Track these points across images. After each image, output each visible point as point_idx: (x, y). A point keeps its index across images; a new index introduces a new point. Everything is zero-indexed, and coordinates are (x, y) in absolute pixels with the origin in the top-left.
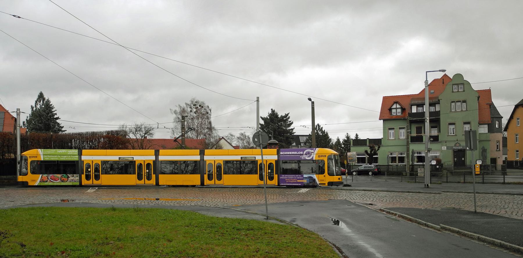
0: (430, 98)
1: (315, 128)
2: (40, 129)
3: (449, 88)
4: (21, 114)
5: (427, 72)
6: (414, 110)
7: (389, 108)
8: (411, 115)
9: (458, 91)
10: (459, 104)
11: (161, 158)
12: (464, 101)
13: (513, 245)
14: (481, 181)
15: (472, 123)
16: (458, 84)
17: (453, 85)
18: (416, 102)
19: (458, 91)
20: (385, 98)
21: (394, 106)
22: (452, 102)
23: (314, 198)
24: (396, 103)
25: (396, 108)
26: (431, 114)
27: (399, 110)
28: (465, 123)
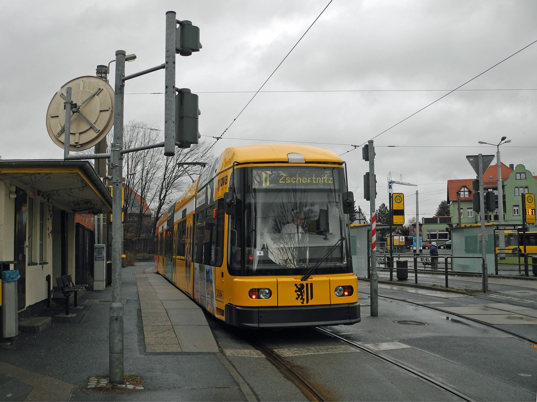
2: (190, 279)
3: (512, 175)
4: (41, 266)
5: (390, 183)
7: (457, 190)
12: (526, 187)
16: (520, 173)
17: (516, 173)
18: (491, 186)
20: (450, 183)
21: (463, 190)
23: (118, 371)
24: (464, 187)
25: (464, 191)
27: (467, 193)
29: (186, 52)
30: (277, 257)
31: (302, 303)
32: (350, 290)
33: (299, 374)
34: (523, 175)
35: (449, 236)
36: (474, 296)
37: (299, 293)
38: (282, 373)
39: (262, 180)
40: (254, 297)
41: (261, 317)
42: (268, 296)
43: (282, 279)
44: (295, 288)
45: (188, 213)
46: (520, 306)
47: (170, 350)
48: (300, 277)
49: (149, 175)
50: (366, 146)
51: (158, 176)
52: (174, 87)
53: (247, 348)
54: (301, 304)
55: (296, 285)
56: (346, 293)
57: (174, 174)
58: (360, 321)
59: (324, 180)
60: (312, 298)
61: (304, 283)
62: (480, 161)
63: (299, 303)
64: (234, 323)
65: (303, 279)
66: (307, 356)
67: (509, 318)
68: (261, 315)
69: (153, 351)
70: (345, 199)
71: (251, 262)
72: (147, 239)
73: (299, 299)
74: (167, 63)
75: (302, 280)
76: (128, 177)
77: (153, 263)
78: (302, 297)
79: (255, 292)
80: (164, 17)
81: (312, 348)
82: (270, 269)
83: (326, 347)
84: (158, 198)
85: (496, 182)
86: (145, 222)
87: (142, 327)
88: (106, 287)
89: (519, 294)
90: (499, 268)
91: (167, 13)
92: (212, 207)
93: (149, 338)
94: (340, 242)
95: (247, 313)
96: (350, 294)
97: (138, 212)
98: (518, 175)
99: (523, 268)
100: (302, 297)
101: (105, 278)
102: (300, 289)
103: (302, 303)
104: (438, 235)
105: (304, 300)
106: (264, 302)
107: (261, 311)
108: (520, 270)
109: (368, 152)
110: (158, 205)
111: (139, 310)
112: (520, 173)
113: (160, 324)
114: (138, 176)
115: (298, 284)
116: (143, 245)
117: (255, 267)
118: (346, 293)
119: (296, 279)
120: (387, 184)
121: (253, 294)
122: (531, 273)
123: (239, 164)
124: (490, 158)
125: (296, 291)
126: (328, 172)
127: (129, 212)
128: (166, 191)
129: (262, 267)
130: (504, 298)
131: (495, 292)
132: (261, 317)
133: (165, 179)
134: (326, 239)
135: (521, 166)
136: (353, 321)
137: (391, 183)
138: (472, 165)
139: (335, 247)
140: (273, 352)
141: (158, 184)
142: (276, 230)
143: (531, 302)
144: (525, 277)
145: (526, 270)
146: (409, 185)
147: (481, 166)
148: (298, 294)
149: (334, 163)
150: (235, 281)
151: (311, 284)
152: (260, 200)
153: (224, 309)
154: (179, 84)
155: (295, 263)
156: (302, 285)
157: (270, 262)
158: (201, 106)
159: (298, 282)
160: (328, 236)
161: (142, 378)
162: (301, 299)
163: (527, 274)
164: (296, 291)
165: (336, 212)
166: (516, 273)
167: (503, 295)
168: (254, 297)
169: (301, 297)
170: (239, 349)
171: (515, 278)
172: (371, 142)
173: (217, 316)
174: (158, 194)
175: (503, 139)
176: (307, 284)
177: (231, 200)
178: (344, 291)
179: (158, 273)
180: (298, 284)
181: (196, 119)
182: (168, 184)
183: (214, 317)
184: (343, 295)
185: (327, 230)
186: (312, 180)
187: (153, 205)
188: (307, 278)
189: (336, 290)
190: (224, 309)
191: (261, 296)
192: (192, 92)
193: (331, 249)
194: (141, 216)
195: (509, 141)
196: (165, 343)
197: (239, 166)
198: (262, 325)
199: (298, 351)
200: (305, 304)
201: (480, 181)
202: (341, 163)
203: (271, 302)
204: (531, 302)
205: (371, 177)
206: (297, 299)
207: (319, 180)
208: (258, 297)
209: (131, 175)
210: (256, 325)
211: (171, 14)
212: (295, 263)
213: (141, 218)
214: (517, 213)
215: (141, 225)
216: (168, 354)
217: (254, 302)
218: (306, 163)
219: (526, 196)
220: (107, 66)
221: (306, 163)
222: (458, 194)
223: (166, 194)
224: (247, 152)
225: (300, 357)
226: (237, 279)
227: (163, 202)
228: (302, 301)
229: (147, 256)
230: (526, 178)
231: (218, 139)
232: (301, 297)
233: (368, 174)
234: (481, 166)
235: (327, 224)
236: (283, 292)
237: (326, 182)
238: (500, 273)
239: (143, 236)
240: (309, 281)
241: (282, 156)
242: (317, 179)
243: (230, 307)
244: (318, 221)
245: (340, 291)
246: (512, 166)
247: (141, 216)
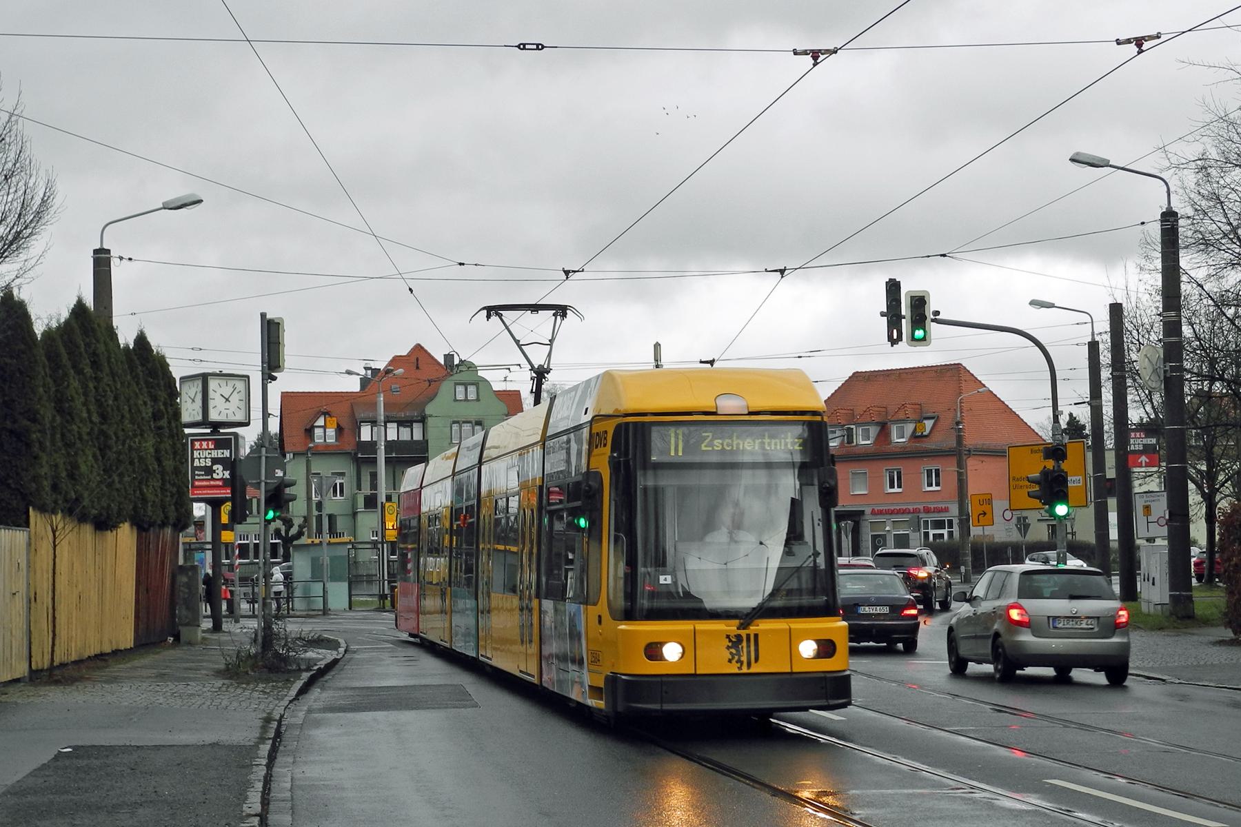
3: (446, 387)
9: (466, 400)
12: (479, 423)
19: (466, 400)
21: (321, 422)
22: (454, 422)
27: (331, 432)
35: (281, 551)
48: (737, 622)
54: (737, 671)
55: (728, 637)
59: (786, 444)
60: (757, 660)
65: (743, 626)
98: (460, 389)
103: (740, 668)
104: (252, 546)
105: (742, 663)
112: (466, 385)
119: (731, 627)
125: (728, 648)
151: (756, 636)
153: (602, 685)
156: (739, 637)
164: (728, 648)
176: (748, 636)
180: (732, 634)
190: (602, 685)
198: (667, 707)
200: (745, 670)
206: (730, 661)
210: (656, 707)
218: (750, 413)
221: (750, 413)
222: (309, 432)
226: (623, 627)
230: (478, 400)
240: (753, 629)
243: (613, 680)
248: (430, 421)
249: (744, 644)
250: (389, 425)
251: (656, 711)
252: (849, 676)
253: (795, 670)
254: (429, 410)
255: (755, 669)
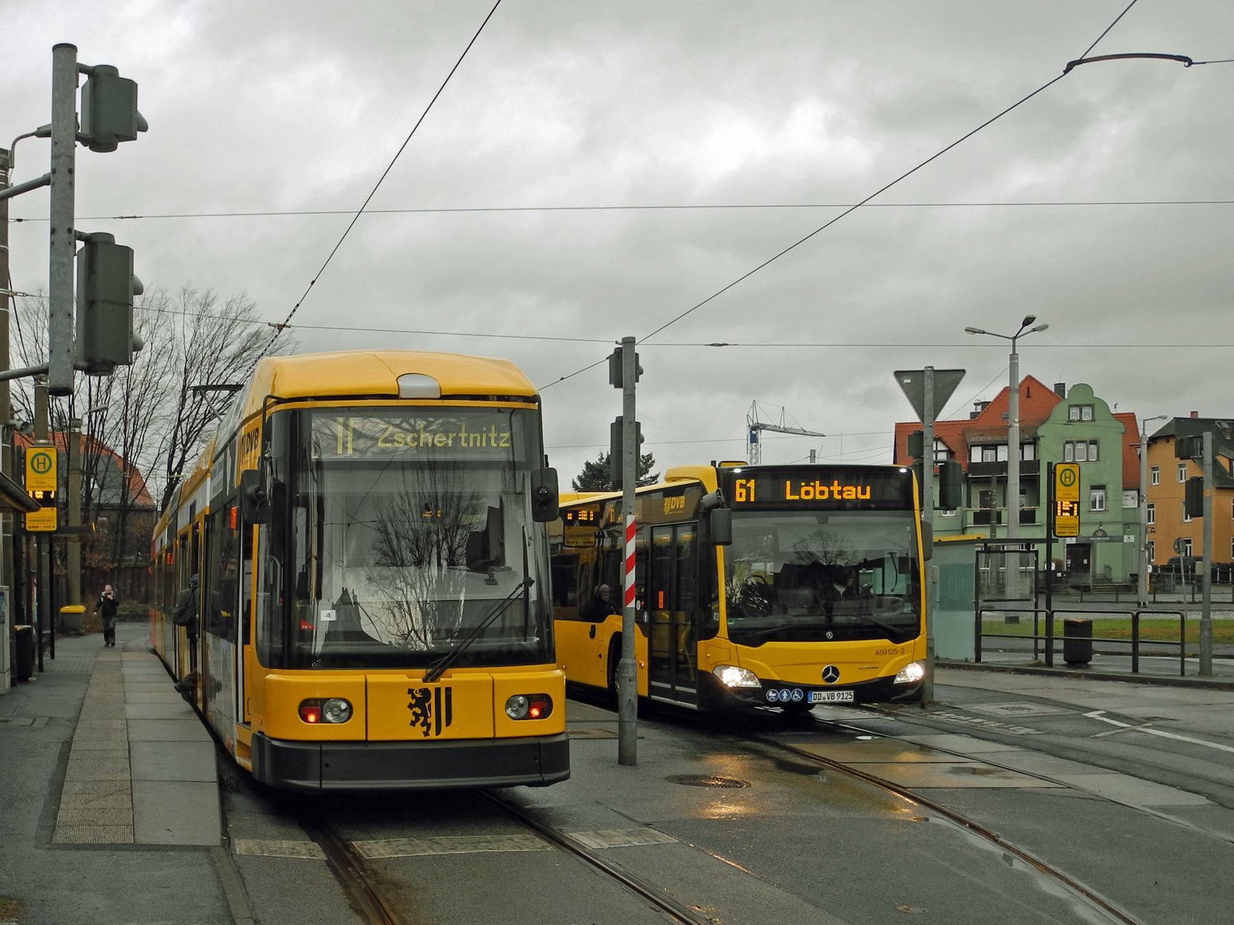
0: (1022, 430)
1: (761, 681)
3: (1059, 412)
6: (977, 456)
8: (974, 467)
9: (1080, 420)
10: (1080, 446)
11: (100, 659)
12: (1094, 442)
13: (679, 703)
14: (1127, 670)
15: (1110, 487)
16: (1080, 407)
17: (1070, 406)
19: (1080, 420)
22: (1068, 442)
26: (1024, 465)
28: (1094, 488)
29: (102, 142)
30: (382, 624)
31: (426, 734)
32: (543, 703)
33: (387, 900)
34: (1086, 410)
36: (896, 715)
37: (418, 711)
38: (349, 895)
39: (336, 439)
40: (312, 718)
41: (327, 765)
42: (344, 715)
43: (377, 677)
44: (409, 699)
45: (198, 510)
46: (995, 741)
47: (108, 840)
48: (422, 672)
49: (143, 412)
50: (618, 352)
51: (164, 413)
52: (70, 231)
53: (285, 837)
54: (422, 737)
55: (411, 691)
56: (535, 712)
57: (202, 410)
58: (566, 777)
60: (448, 722)
61: (431, 686)
62: (929, 384)
63: (417, 733)
64: (268, 778)
66: (422, 858)
67: (958, 771)
68: (325, 760)
69: (68, 841)
70: (537, 485)
71: (308, 636)
72: (140, 568)
73: (418, 724)
74: (54, 171)
75: (425, 681)
76: (90, 417)
77: (149, 626)
78: (426, 720)
79: (312, 706)
80: (50, 55)
81: (444, 839)
82: (359, 654)
83: (477, 838)
84: (165, 467)
85: (1006, 430)
86: (135, 526)
87: (61, 785)
88: (13, 684)
89: (1003, 713)
90: (985, 642)
91: (56, 48)
92: (232, 501)
93: (69, 810)
94: (522, 589)
95: (290, 757)
96: (544, 714)
97: (116, 501)
98: (1075, 411)
99: (1042, 644)
100: (426, 720)
101: (8, 665)
102: (420, 701)
103: (426, 734)
105: (429, 726)
106: (333, 730)
107: (328, 752)
108: (1036, 651)
109: (624, 367)
110: (165, 484)
111: (68, 744)
112: (1080, 407)
113: (104, 777)
114: (113, 416)
115: (416, 689)
116: (129, 582)
117: (318, 646)
118: (535, 712)
119: (413, 678)
120: (745, 433)
121: (312, 712)
122: (1058, 659)
123: (280, 401)
124: (955, 375)
125: (411, 706)
126: (505, 417)
127: (96, 501)
128: (185, 452)
129: (341, 647)
130: (964, 720)
131: (950, 708)
132: (327, 765)
133: (180, 422)
134: (491, 582)
135: (1083, 388)
136: (547, 777)
137: (756, 428)
138: (907, 394)
139: (509, 600)
140: (348, 847)
141: (163, 432)
142: (385, 554)
143: (1024, 731)
144: (1044, 669)
145: (1049, 651)
146: (805, 433)
147: (929, 397)
148: (414, 713)
149: (501, 398)
150: (271, 682)
151: (448, 690)
152: (332, 487)
154: (83, 225)
155: (429, 637)
156: (426, 693)
157: (362, 636)
158: (141, 270)
159: (417, 683)
160: (498, 575)
161: (21, 902)
162: (422, 725)
163: (1049, 663)
164: (411, 706)
165: (520, 518)
166: (1029, 658)
167: (967, 713)
168: (312, 718)
169: (422, 719)
170: (273, 838)
171: (1019, 671)
172: (629, 342)
173: (239, 759)
174: (166, 457)
175: (1028, 321)
176: (438, 690)
177: (258, 490)
178: (530, 708)
179: (154, 652)
180: (416, 689)
181: (127, 306)
182: (188, 435)
183: (234, 761)
184: (528, 716)
185: (500, 560)
186: (457, 440)
187: (156, 486)
188: (439, 675)
189: (509, 704)
191: (329, 717)
192: (118, 241)
193: (503, 605)
194: (125, 510)
195: (1044, 328)
196: (100, 822)
197: (281, 407)
198: (328, 785)
199: (409, 848)
200: (432, 735)
201: (925, 435)
202: (535, 399)
203: (351, 731)
204: (1024, 731)
205: (627, 430)
206: (413, 724)
207: (475, 439)
208: (321, 719)
209: (196, 389)
210: (314, 784)
211: (65, 51)
212: (429, 637)
213: (124, 517)
214: (1101, 506)
215: (124, 533)
216: (102, 847)
217: (312, 730)
218: (443, 397)
219: (1060, 468)
220: (9, 148)
221: (443, 397)
223: (183, 457)
224: (298, 372)
225: (405, 860)
226: (274, 676)
227: (178, 479)
228: (425, 729)
229: (140, 608)
230: (1093, 420)
231: (280, 327)
232: (422, 719)
233: (620, 420)
234: (929, 397)
235: (502, 545)
236: (381, 708)
237: (493, 444)
238: (986, 658)
239: (130, 559)
240: (443, 681)
241: (382, 381)
242: (472, 436)
244: (485, 534)
245: (521, 706)
246: (1060, 387)
247: (125, 510)
248: (1042, 442)
249: (433, 701)
250: (1026, 447)
251: (314, 790)
252: (566, 743)
253: (498, 735)
254: (1040, 432)
255: (446, 733)
